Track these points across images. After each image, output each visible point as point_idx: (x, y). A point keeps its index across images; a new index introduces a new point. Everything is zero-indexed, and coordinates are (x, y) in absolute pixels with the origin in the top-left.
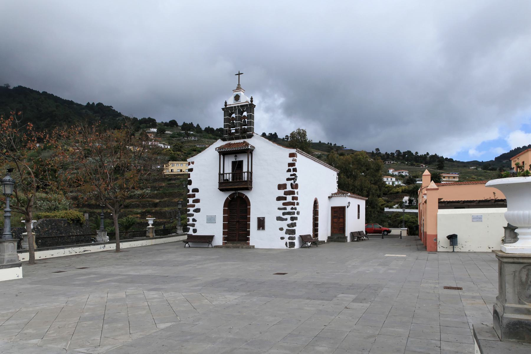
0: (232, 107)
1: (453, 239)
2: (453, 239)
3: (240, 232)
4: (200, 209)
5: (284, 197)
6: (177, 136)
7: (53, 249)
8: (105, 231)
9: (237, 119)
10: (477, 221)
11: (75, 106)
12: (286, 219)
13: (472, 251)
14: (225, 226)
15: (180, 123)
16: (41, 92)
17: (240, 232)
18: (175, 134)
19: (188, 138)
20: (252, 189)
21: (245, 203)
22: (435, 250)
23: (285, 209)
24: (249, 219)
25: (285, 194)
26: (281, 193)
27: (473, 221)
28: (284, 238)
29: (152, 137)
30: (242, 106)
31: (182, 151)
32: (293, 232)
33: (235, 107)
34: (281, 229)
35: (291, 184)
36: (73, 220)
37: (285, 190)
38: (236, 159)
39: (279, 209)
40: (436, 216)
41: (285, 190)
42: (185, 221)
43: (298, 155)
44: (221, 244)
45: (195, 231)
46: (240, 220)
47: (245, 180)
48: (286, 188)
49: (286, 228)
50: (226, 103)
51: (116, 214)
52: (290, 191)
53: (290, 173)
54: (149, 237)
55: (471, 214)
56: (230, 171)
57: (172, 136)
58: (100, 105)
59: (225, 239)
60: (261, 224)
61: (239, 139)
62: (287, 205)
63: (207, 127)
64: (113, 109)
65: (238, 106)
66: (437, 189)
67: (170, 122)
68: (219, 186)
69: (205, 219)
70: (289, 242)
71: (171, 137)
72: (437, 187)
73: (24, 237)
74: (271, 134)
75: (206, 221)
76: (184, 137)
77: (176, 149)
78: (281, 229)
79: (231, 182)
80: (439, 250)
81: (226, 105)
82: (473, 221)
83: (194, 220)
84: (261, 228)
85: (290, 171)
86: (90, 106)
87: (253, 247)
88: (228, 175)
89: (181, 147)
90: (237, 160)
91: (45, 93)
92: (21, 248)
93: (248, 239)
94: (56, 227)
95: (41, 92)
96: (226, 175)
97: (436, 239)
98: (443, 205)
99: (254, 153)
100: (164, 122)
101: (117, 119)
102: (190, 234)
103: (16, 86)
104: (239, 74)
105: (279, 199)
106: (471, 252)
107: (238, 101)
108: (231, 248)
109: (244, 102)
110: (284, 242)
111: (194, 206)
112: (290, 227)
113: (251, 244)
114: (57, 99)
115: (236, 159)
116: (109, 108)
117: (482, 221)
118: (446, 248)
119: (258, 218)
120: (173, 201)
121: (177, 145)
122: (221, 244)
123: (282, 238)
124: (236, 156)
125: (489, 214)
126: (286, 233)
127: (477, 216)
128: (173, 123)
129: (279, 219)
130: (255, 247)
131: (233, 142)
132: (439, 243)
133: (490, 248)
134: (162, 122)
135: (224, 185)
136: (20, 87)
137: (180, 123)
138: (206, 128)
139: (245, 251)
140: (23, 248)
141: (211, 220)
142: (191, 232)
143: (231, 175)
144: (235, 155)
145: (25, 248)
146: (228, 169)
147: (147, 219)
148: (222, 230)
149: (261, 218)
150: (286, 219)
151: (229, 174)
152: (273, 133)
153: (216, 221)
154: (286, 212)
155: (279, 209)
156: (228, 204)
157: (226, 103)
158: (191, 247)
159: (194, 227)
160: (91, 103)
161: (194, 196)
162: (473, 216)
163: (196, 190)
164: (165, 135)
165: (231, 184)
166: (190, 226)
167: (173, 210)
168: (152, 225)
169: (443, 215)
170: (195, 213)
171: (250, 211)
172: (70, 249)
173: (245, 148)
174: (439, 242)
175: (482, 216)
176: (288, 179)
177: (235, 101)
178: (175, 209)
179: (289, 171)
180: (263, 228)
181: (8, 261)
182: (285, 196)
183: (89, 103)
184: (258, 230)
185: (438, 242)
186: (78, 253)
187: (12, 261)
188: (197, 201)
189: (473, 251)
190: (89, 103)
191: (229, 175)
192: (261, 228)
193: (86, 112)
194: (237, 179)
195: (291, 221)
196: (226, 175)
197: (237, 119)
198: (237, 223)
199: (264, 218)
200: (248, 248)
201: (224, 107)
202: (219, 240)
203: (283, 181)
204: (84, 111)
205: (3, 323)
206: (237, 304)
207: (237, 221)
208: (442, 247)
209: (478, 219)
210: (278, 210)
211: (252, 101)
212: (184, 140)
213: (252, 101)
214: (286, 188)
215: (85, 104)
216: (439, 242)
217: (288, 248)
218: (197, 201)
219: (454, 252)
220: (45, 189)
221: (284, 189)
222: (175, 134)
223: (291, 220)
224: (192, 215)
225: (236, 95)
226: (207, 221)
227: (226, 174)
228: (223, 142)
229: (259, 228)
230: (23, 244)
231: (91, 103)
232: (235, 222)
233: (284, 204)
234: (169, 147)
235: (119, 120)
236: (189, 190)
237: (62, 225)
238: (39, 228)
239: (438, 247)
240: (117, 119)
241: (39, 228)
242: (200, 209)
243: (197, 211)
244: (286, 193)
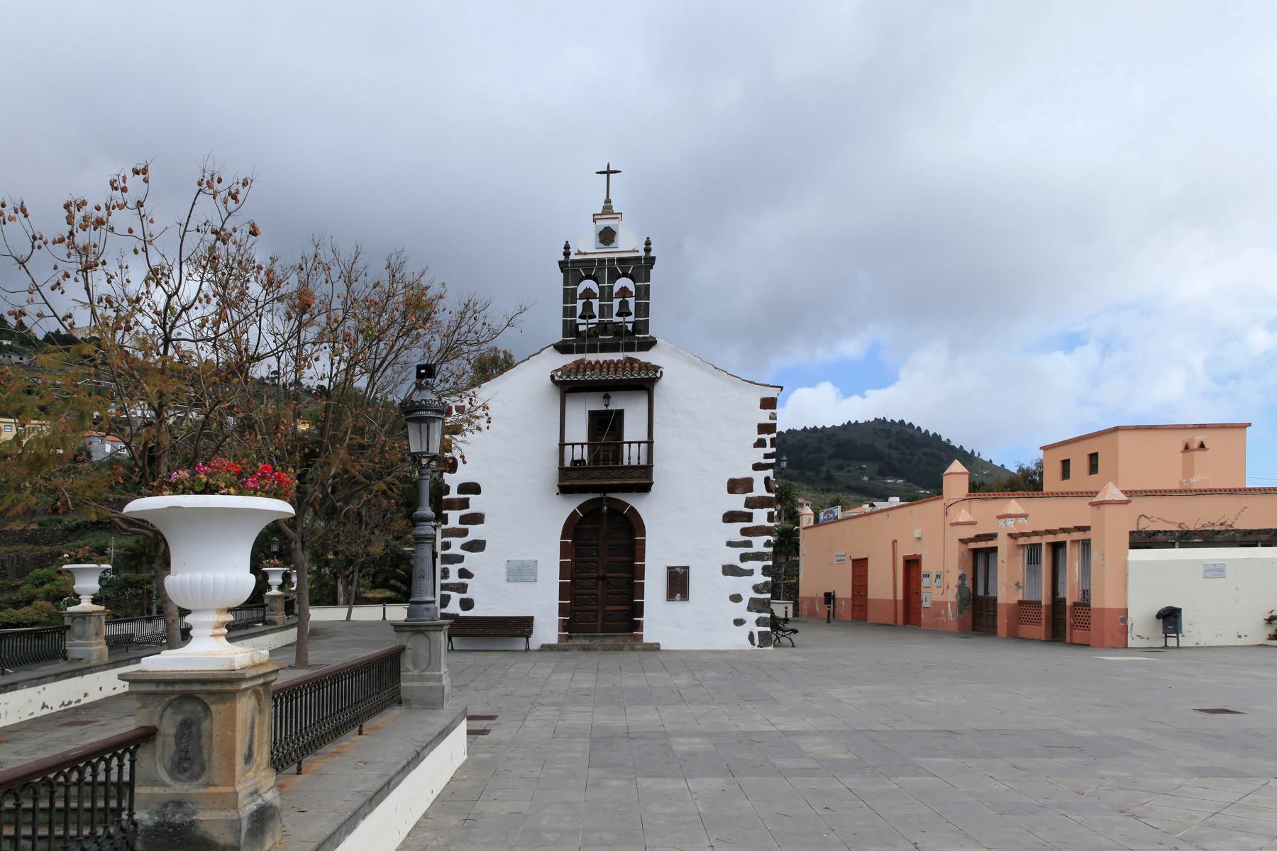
0: (593, 261)
1: (1170, 618)
2: (1170, 618)
3: (608, 608)
5: (745, 513)
9: (606, 296)
10: (1215, 577)
12: (750, 573)
13: (1202, 644)
14: (564, 591)
17: (608, 608)
20: (653, 487)
21: (632, 527)
22: (1121, 643)
23: (748, 544)
24: (640, 572)
25: (747, 505)
26: (737, 502)
28: (745, 622)
30: (621, 260)
33: (601, 261)
34: (736, 598)
35: (767, 480)
37: (750, 495)
38: (607, 406)
39: (730, 544)
40: (1126, 562)
41: (750, 495)
42: (57, 586)
44: (553, 640)
45: (467, 604)
46: (609, 575)
47: (641, 464)
48: (751, 490)
49: (748, 594)
50: (567, 247)
51: (303, 550)
52: (763, 497)
53: (762, 451)
54: (274, 623)
55: (1201, 561)
56: (584, 439)
59: (564, 626)
60: (678, 583)
61: (617, 350)
62: (754, 535)
65: (611, 260)
66: (1126, 502)
69: (503, 572)
70: (760, 633)
72: (1126, 498)
73: (76, 620)
75: (504, 577)
78: (736, 598)
80: (1131, 644)
81: (567, 254)
82: (1205, 577)
83: (464, 573)
84: (678, 595)
85: (764, 446)
87: (655, 648)
88: (634, 446)
90: (609, 408)
92: (66, 659)
93: (639, 626)
96: (630, 446)
97: (1125, 620)
98: (1142, 540)
99: (658, 390)
102: (451, 612)
104: (608, 172)
105: (730, 517)
106: (1203, 647)
107: (612, 245)
108: (596, 650)
109: (629, 251)
110: (744, 631)
111: (464, 533)
112: (761, 593)
113: (646, 640)
115: (607, 406)
117: (1224, 577)
118: (1148, 638)
119: (669, 568)
120: (6, 529)
122: (553, 640)
123: (739, 622)
124: (607, 397)
125: (1239, 561)
126: (750, 609)
127: (1215, 565)
129: (730, 570)
131: (592, 357)
132: (1131, 628)
133: (1240, 637)
135: (575, 474)
139: (628, 658)
140: (73, 659)
141: (521, 573)
142: (454, 607)
143: (586, 447)
144: (603, 394)
145: (80, 656)
146: (578, 430)
147: (263, 569)
148: (556, 601)
149: (678, 570)
150: (750, 573)
151: (639, 443)
153: (536, 576)
154: (749, 554)
155: (730, 544)
156: (574, 529)
157: (567, 247)
158: (456, 650)
159: (465, 592)
161: (464, 504)
162: (1205, 565)
163: (474, 488)
166: (451, 590)
167: (11, 555)
169: (1140, 563)
170: (467, 554)
171: (645, 549)
173: (568, 379)
174: (1132, 625)
175: (1224, 564)
176: (757, 467)
177: (602, 246)
178: (17, 551)
179: (760, 444)
184: (667, 600)
185: (1129, 626)
188: (477, 519)
189: (1204, 645)
191: (639, 446)
192: (678, 595)
194: (606, 460)
195: (763, 577)
196: (630, 446)
197: (606, 296)
198: (600, 582)
200: (651, 650)
201: (562, 258)
202: (547, 629)
203: (745, 472)
205: (1220, 809)
206: (544, 808)
207: (599, 577)
208: (1138, 636)
209: (1216, 571)
210: (728, 547)
211: (648, 250)
213: (648, 250)
214: (751, 490)
216: (1132, 625)
217: (756, 647)
218: (477, 519)
219: (1180, 648)
220: (243, 468)
221: (744, 493)
223: (763, 574)
224: (460, 559)
225: (606, 228)
226: (508, 576)
227: (630, 443)
228: (560, 355)
229: (671, 596)
230: (71, 646)
232: (594, 581)
233: (744, 532)
236: (448, 487)
239: (1129, 637)
243: (477, 546)
244: (752, 503)
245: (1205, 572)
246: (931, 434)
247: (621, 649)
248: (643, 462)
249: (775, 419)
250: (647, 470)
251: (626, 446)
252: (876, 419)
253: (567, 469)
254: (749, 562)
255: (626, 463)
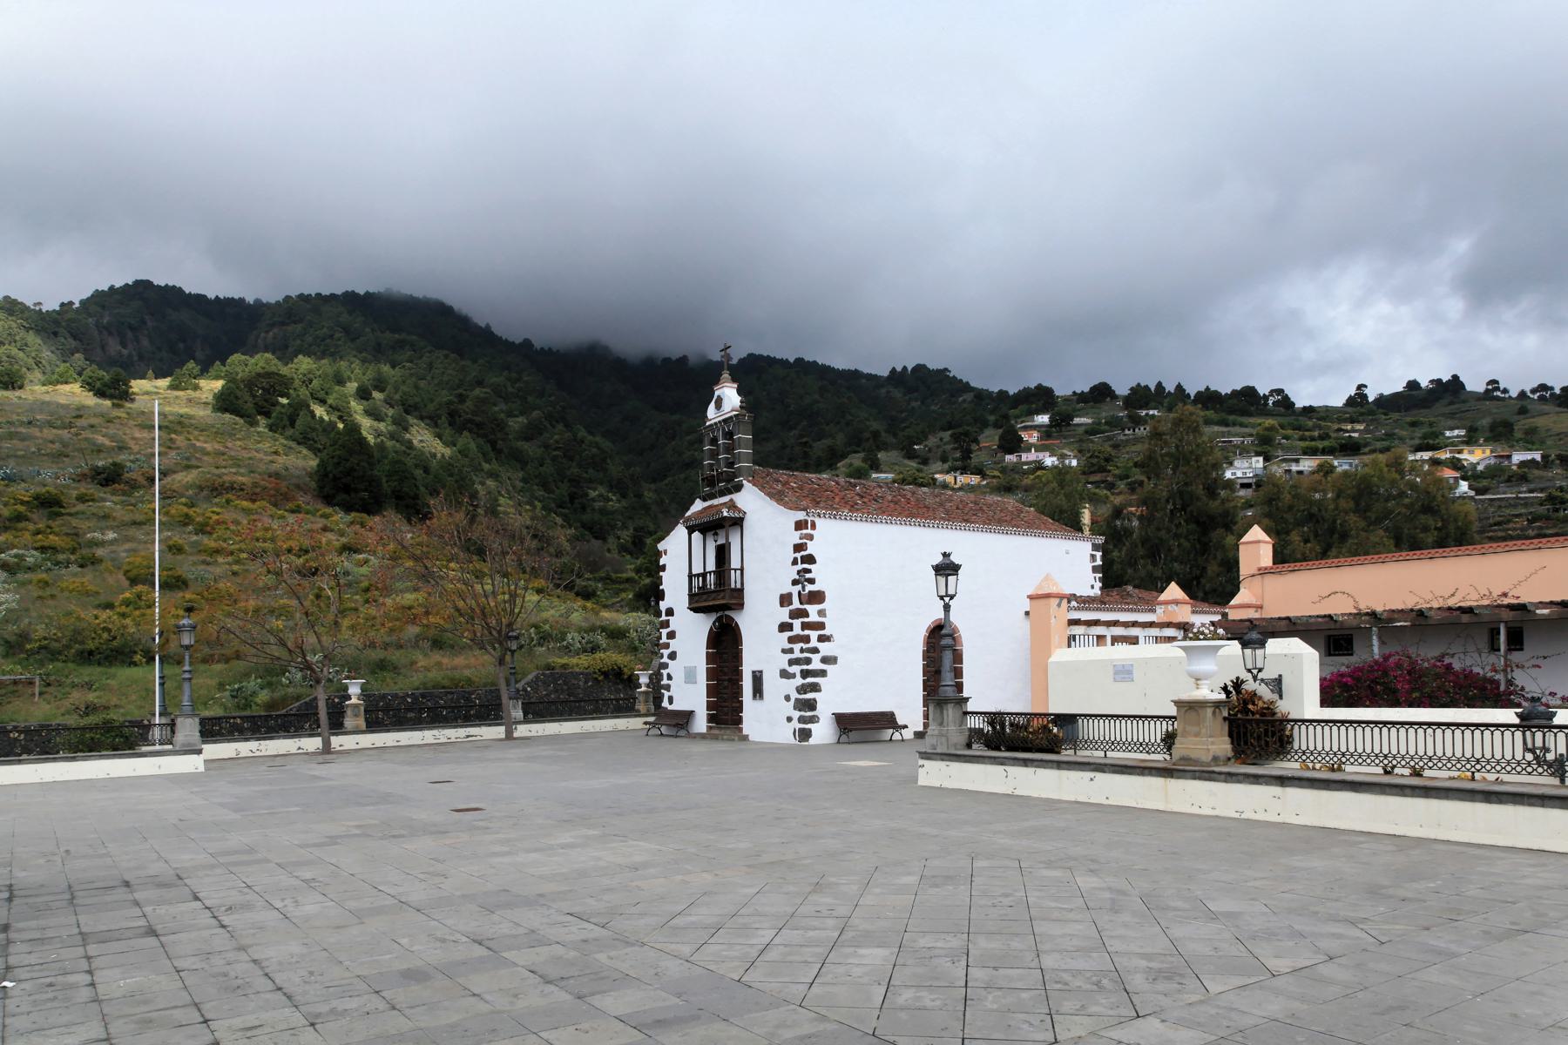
4: (1322, 706)
6: (1107, 428)
7: (399, 730)
8: (517, 699)
11: (864, 381)
15: (1122, 390)
16: (792, 360)
18: (1100, 424)
19: (1137, 430)
23: (791, 651)
27: (1115, 680)
29: (1032, 437)
31: (1109, 471)
32: (811, 705)
36: (606, 674)
37: (791, 607)
41: (791, 607)
43: (818, 521)
44: (704, 730)
55: (1112, 661)
57: (1091, 431)
58: (919, 368)
59: (711, 719)
63: (1202, 389)
64: (951, 375)
67: (1094, 389)
68: (690, 604)
71: (1086, 432)
74: (1439, 381)
76: (1123, 430)
77: (1093, 465)
79: (714, 592)
82: (1115, 680)
86: (897, 377)
89: (1107, 460)
91: (799, 361)
93: (739, 721)
94: (565, 687)
95: (792, 360)
99: (745, 524)
100: (1079, 391)
101: (961, 399)
103: (744, 355)
114: (824, 372)
116: (942, 373)
121: (1096, 454)
122: (704, 730)
128: (1102, 392)
130: (750, 738)
134: (1074, 392)
136: (751, 355)
137: (1122, 390)
138: (1199, 393)
150: (793, 676)
152: (1446, 378)
160: (899, 369)
164: (1073, 428)
165: (713, 595)
168: (648, 686)
172: (435, 732)
175: (1132, 665)
180: (761, 697)
181: (184, 745)
182: (790, 621)
183: (894, 368)
186: (453, 740)
187: (189, 745)
190: (894, 368)
193: (888, 392)
199: (761, 672)
202: (701, 724)
203: (788, 588)
204: (883, 391)
212: (1124, 438)
215: (885, 373)
222: (1100, 424)
229: (754, 697)
231: (899, 369)
234: (1074, 463)
235: (964, 401)
237: (581, 683)
238: (529, 689)
240: (961, 399)
241: (529, 689)
242: (1322, 706)
245: (1115, 674)
246: (1153, 389)
247: (733, 740)
248: (739, 586)
249: (825, 616)
250: (740, 591)
251: (733, 572)
252: (967, 383)
253: (695, 595)
254: (865, 372)
255: (733, 586)
